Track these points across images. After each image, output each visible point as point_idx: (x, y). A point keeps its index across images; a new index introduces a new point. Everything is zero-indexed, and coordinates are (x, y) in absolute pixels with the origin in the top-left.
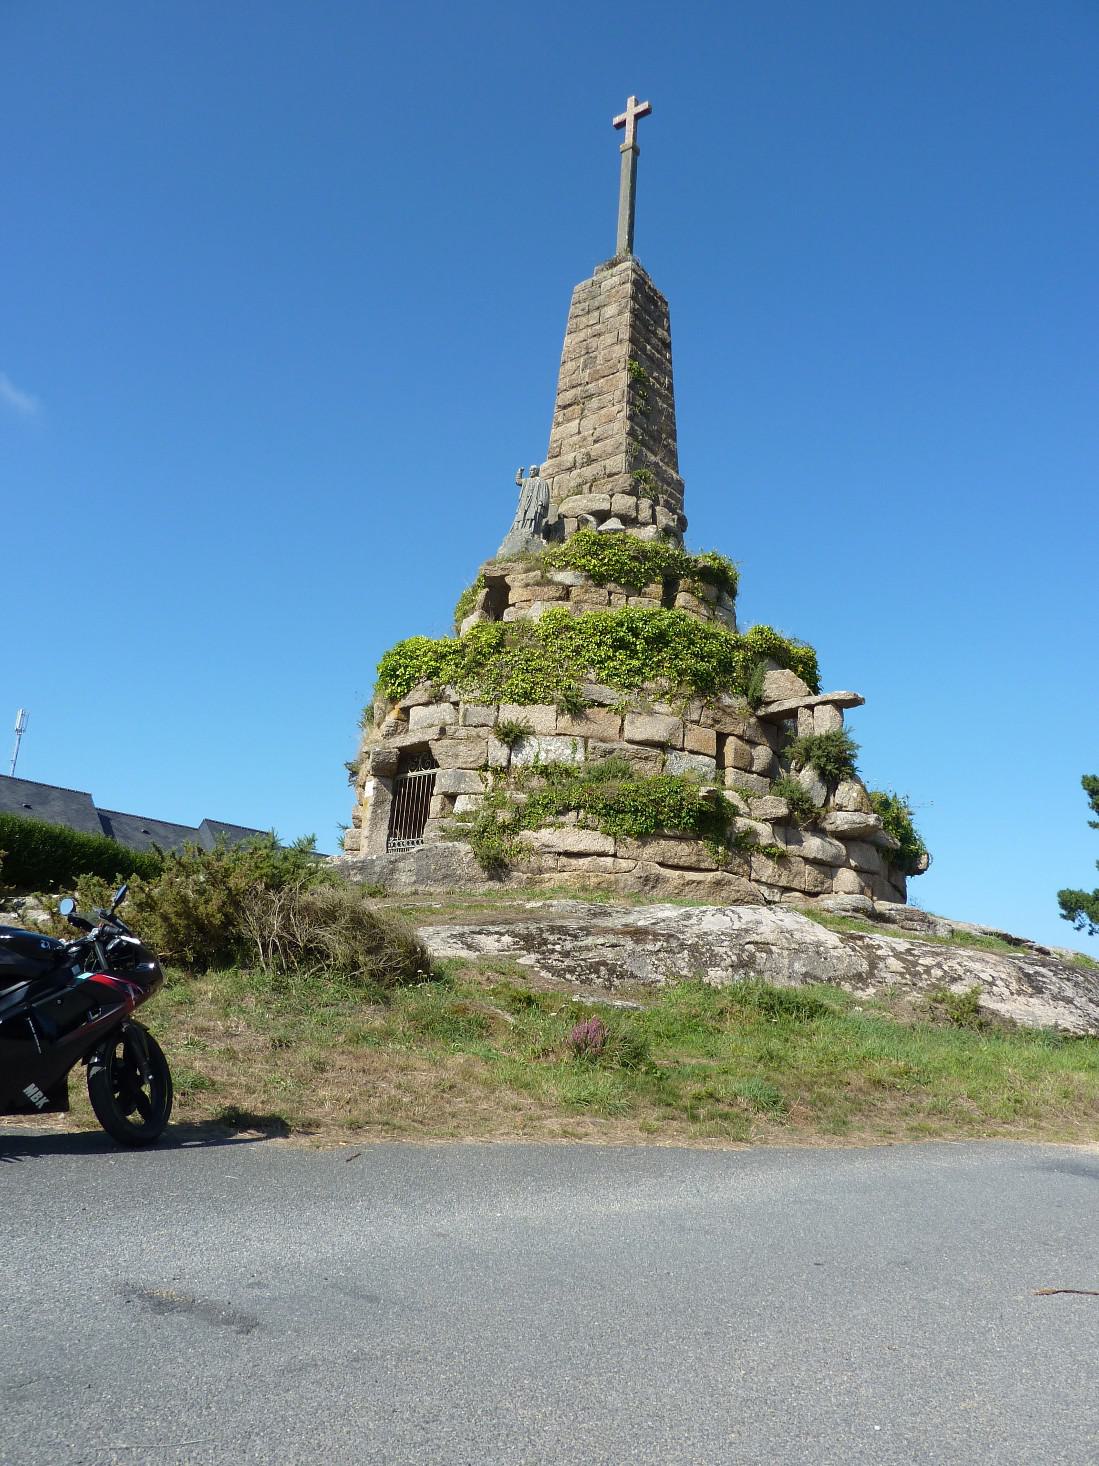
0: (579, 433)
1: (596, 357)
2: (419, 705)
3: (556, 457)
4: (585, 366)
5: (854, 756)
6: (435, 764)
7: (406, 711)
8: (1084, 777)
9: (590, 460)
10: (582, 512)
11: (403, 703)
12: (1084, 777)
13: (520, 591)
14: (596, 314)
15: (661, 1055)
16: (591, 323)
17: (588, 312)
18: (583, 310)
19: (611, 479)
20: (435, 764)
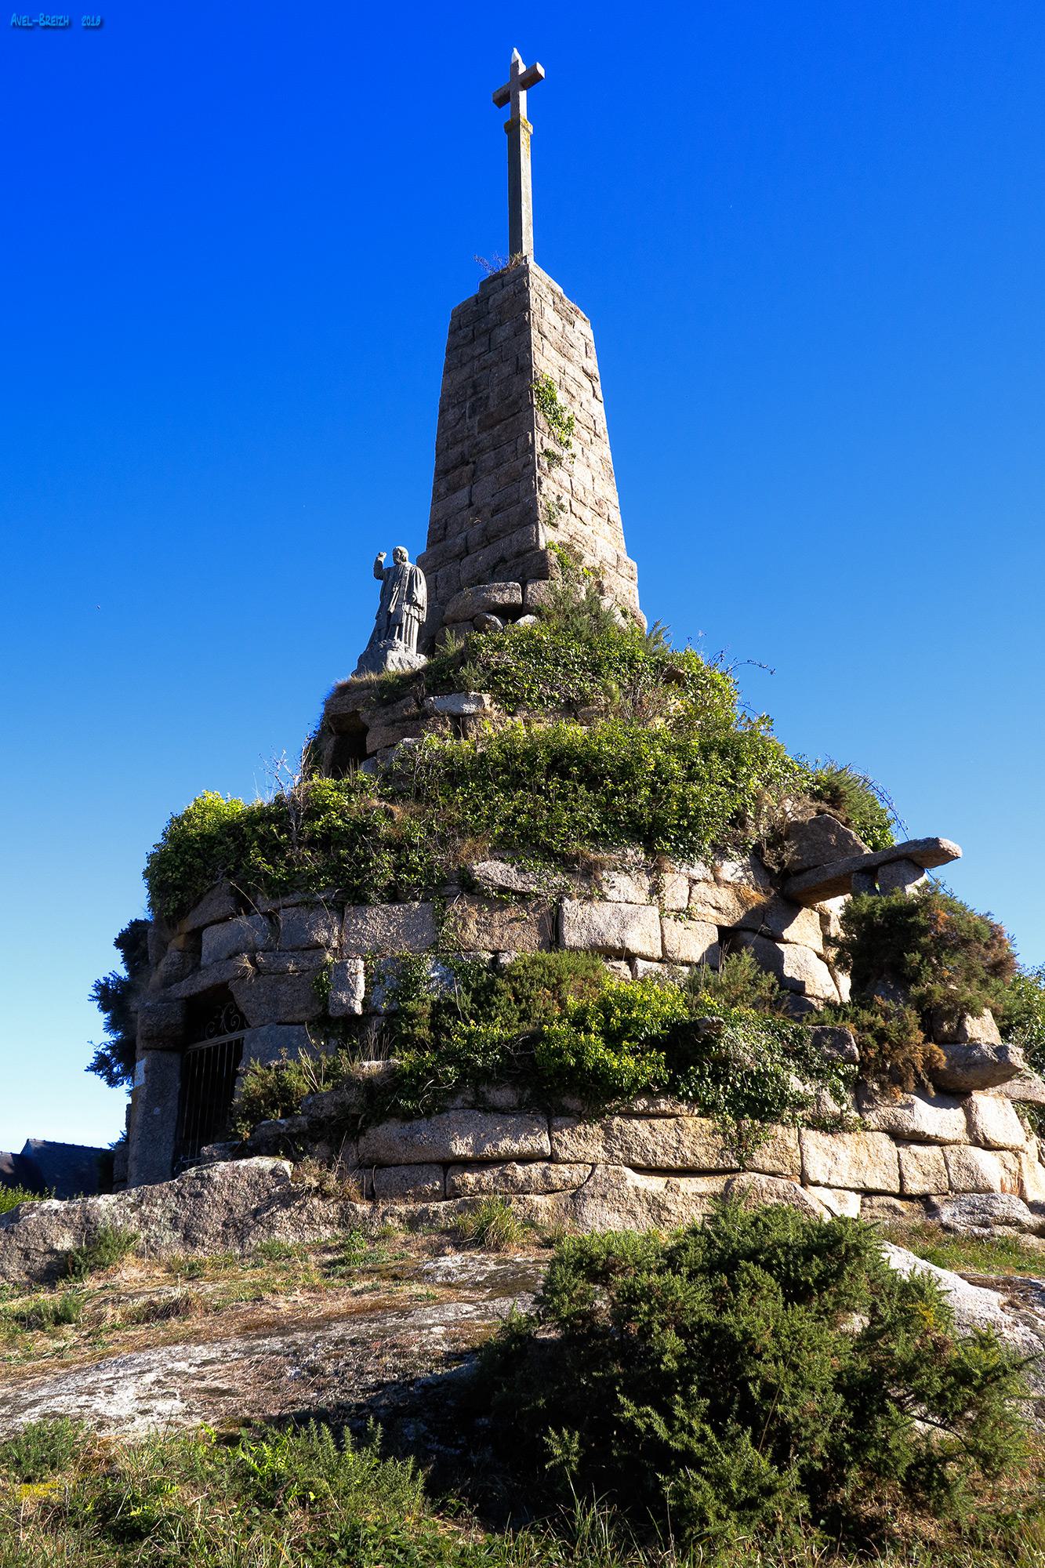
0: (471, 504)
1: (488, 397)
2: (213, 923)
3: (440, 541)
4: (474, 411)
5: (14, 1155)
6: (243, 1024)
7: (196, 934)
8: (94, 1068)
9: (488, 539)
10: (479, 611)
11: (189, 924)
12: (94, 1068)
13: (384, 730)
14: (484, 339)
15: (659, 953)
16: (476, 353)
17: (473, 340)
18: (464, 337)
19: (520, 560)
20: (243, 1024)
